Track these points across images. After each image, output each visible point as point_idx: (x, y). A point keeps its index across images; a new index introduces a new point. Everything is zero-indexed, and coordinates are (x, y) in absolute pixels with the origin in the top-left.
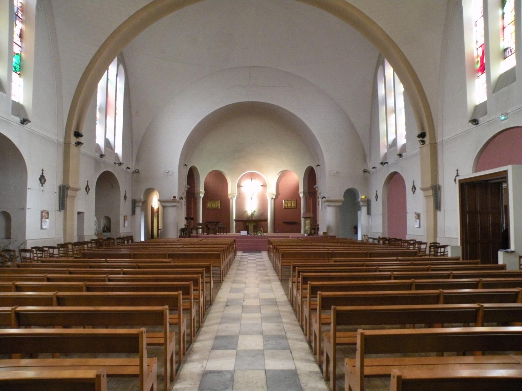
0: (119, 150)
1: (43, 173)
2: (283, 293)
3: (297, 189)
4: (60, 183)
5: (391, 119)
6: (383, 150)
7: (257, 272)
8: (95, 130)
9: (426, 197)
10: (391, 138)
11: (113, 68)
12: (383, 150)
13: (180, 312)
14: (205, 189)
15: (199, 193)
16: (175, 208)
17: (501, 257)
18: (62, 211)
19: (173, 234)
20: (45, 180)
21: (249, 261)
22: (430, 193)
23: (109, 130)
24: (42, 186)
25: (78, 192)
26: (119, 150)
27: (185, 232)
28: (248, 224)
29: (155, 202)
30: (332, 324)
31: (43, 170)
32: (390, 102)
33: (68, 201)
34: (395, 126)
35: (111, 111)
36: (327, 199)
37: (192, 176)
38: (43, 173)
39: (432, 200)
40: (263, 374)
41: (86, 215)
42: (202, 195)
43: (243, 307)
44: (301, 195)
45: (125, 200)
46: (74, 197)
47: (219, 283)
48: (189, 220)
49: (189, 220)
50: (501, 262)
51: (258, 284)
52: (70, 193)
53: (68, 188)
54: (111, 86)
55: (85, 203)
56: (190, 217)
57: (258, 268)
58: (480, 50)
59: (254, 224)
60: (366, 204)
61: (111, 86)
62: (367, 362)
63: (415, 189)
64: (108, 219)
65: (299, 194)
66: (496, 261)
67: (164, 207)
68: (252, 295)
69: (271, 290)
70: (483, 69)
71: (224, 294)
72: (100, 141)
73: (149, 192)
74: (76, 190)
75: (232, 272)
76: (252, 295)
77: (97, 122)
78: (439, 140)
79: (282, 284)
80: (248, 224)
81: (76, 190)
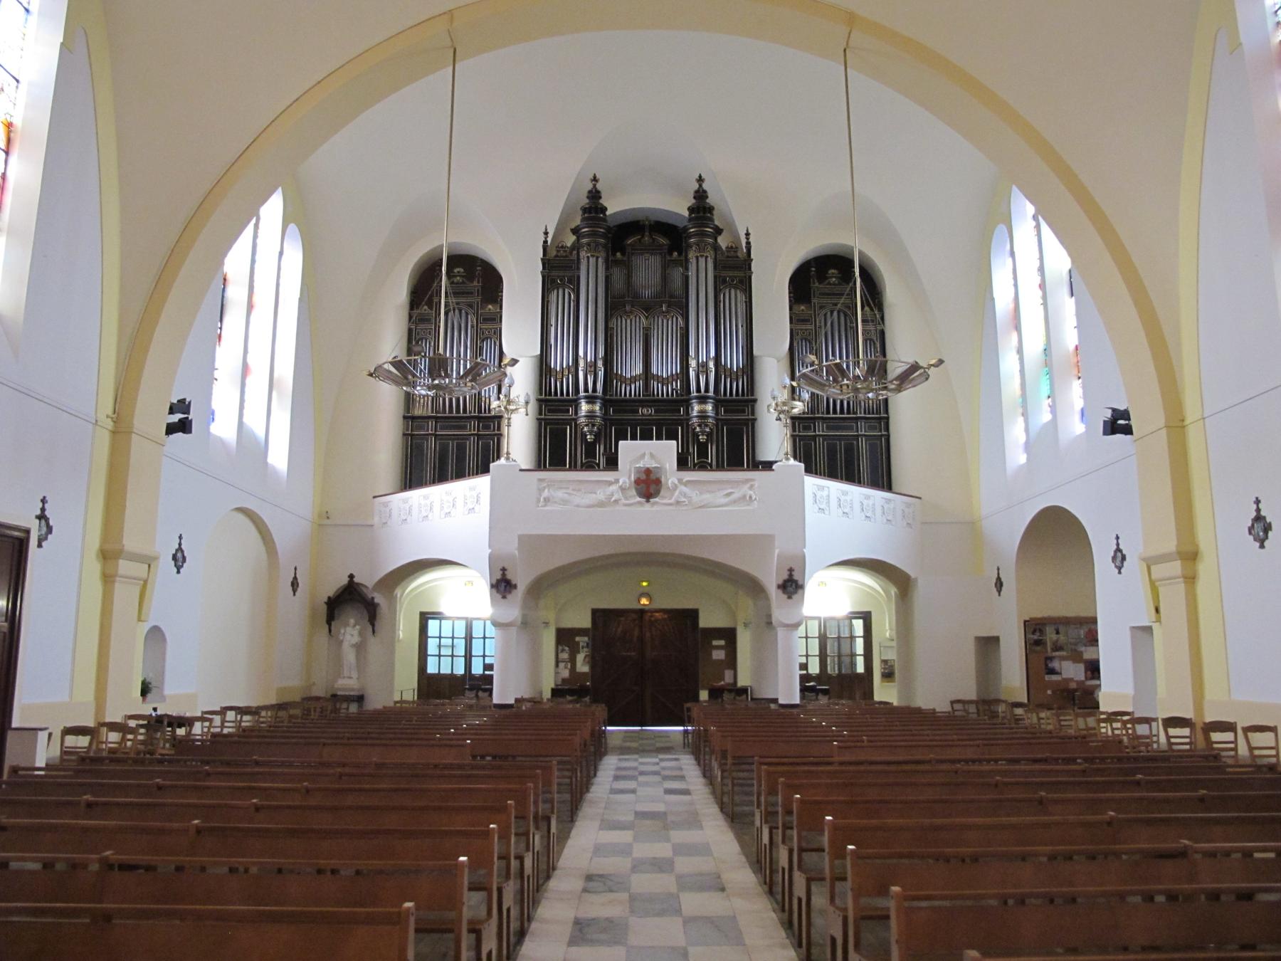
0: (279, 457)
6: (1017, 457)
20: (184, 559)
24: (178, 572)
26: (279, 457)
74: (149, 561)
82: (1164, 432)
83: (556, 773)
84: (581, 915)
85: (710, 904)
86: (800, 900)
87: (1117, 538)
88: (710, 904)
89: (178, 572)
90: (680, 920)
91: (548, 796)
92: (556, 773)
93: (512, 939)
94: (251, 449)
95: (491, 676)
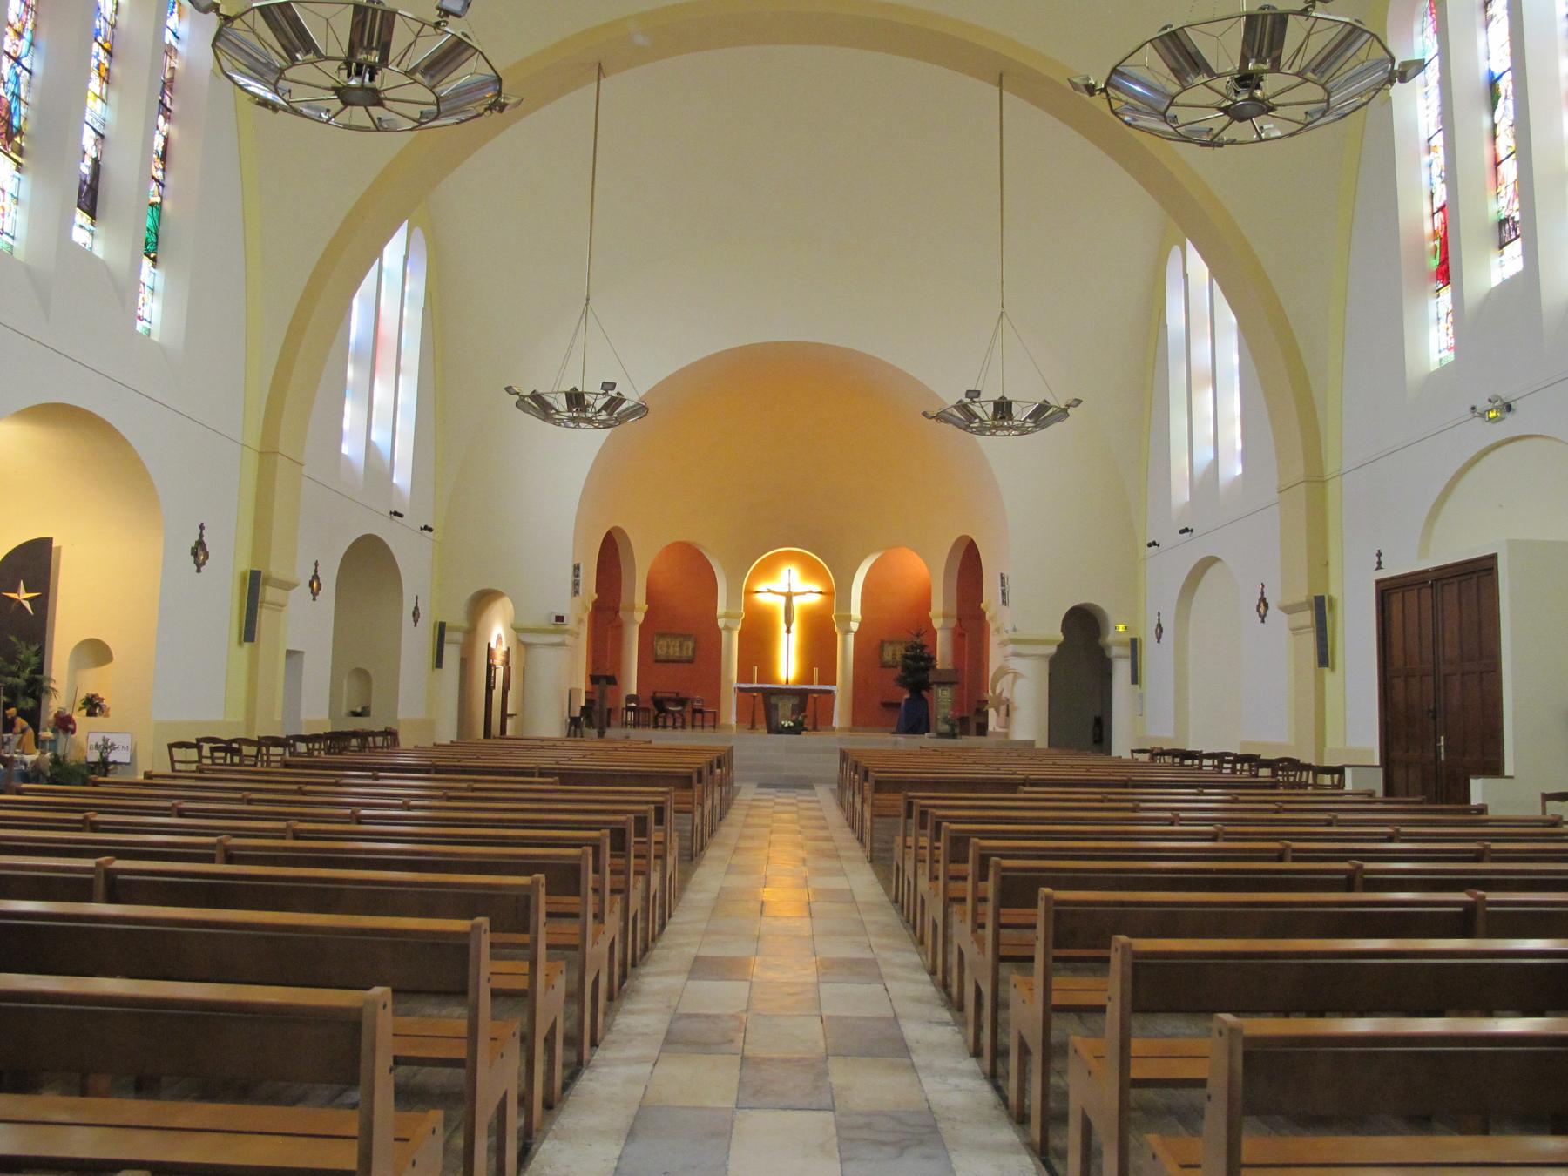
0: (402, 477)
1: (201, 535)
2: (873, 878)
3: (927, 605)
4: (245, 566)
5: (1204, 399)
6: (1181, 493)
7: (802, 846)
8: (340, 414)
9: (1295, 630)
10: (1204, 455)
11: (394, 251)
12: (1181, 493)
13: (585, 924)
14: (650, 598)
15: (632, 608)
16: (561, 651)
17: (1479, 790)
18: (247, 645)
19: (549, 722)
20: (207, 556)
21: (777, 808)
22: (1307, 617)
23: (380, 416)
24: (199, 571)
25: (292, 592)
26: (402, 477)
27: (592, 715)
28: (774, 700)
29: (497, 633)
30: (970, 879)
31: (202, 527)
32: (1202, 351)
33: (264, 615)
34: (1212, 420)
35: (386, 361)
36: (1012, 635)
37: (611, 553)
38: (201, 535)
39: (1310, 640)
40: (816, 1027)
41: (307, 661)
42: (639, 617)
43: (744, 1059)
44: (937, 623)
45: (416, 622)
46: (279, 606)
47: (692, 855)
48: (603, 682)
49: (603, 682)
50: (1476, 798)
51: (806, 879)
52: (269, 593)
53: (268, 580)
54: (391, 293)
55: (306, 623)
56: (603, 678)
57: (803, 822)
58: (1439, 217)
59: (795, 700)
60: (1127, 652)
61: (391, 293)
62: (1059, 981)
63: (1266, 606)
64: (362, 675)
65: (929, 621)
66: (1467, 799)
67: (525, 646)
68: (785, 899)
69: (841, 872)
70: (1443, 274)
71: (709, 879)
72: (351, 448)
73: (482, 600)
74: (288, 586)
75: (729, 831)
76: (785, 899)
77: (348, 393)
78: (1331, 468)
79: (874, 868)
80: (774, 700)
81: (288, 586)
82: (1302, 487)
83: (633, 839)
84: (701, 953)
85: (870, 1087)
86: (935, 926)
87: (1379, 554)
88: (870, 1087)
89: (199, 571)
90: (818, 1124)
91: (569, 927)
92: (633, 839)
93: (638, 952)
94: (377, 466)
95: (830, 692)
